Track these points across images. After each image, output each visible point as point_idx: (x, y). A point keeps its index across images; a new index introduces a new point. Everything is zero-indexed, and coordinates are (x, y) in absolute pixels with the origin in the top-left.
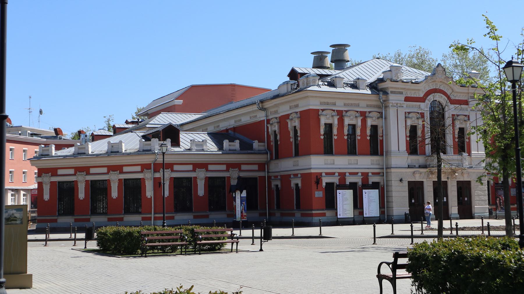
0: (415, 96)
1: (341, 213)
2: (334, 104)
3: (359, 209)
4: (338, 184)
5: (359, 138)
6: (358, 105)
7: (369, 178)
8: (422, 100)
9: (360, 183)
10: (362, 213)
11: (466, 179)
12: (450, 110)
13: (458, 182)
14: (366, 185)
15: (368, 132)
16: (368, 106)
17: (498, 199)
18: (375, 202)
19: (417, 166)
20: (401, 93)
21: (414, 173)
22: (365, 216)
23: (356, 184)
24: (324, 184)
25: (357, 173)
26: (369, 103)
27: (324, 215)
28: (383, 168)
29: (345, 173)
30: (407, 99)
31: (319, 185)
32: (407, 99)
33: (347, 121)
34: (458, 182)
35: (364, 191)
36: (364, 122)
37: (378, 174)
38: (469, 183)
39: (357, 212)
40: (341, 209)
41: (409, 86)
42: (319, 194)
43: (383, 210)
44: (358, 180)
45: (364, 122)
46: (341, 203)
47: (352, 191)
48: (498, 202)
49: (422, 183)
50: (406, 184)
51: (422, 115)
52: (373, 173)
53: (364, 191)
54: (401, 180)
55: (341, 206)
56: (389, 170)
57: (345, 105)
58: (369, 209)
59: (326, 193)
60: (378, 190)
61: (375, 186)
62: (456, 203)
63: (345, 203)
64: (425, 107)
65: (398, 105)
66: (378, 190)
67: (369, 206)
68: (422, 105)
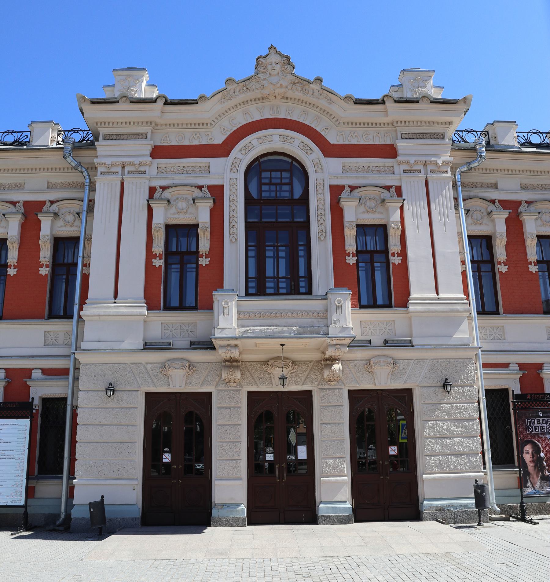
0: (196, 142)
2: (495, 186)
4: (518, 391)
5: (504, 269)
6: (20, 187)
8: (223, 150)
11: (383, 380)
12: (324, 173)
13: (355, 396)
15: (46, 254)
16: (50, 187)
17: (528, 448)
18: (12, 457)
19: (377, 340)
20: (143, 136)
21: (164, 366)
25: (506, 365)
26: (57, 178)
29: (31, 370)
30: (158, 152)
32: (158, 152)
33: (47, 228)
34: (355, 396)
36: (515, 225)
38: (405, 397)
41: (155, 112)
45: (515, 225)
48: (528, 458)
49: (205, 399)
51: (217, 193)
52: (46, 372)
57: (50, 187)
60: (27, 422)
62: (345, 466)
64: (229, 173)
65: (127, 169)
66: (27, 422)
68: (216, 164)
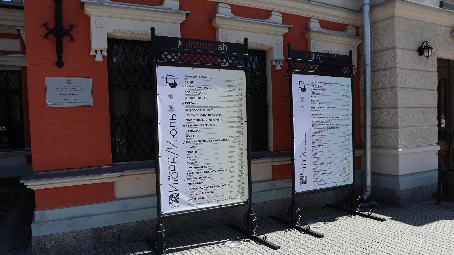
1: (182, 184)
3: (273, 155)
7: (313, 35)
9: (278, 54)
10: (286, 172)
14: (301, 58)
18: (337, 126)
22: (299, 188)
23: (261, 55)
24: (99, 44)
27: (106, 193)
28: (361, 10)
31: (69, 49)
35: (296, 78)
37: (339, 28)
39: (264, 168)
40: (182, 167)
42: (67, 93)
43: (358, 153)
44: (267, 37)
46: (182, 135)
47: (241, 75)
50: (433, 66)
53: (296, 78)
54: (421, 51)
55: (182, 149)
56: (381, 13)
58: (315, 157)
59: (113, 87)
61: (331, 66)
63: (204, 133)
67: (317, 145)
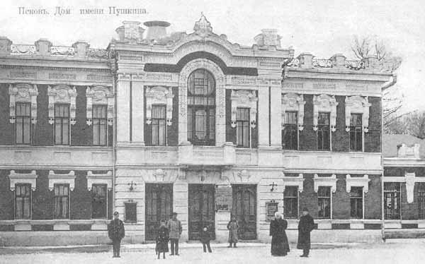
8: (176, 69)
51: (175, 90)
